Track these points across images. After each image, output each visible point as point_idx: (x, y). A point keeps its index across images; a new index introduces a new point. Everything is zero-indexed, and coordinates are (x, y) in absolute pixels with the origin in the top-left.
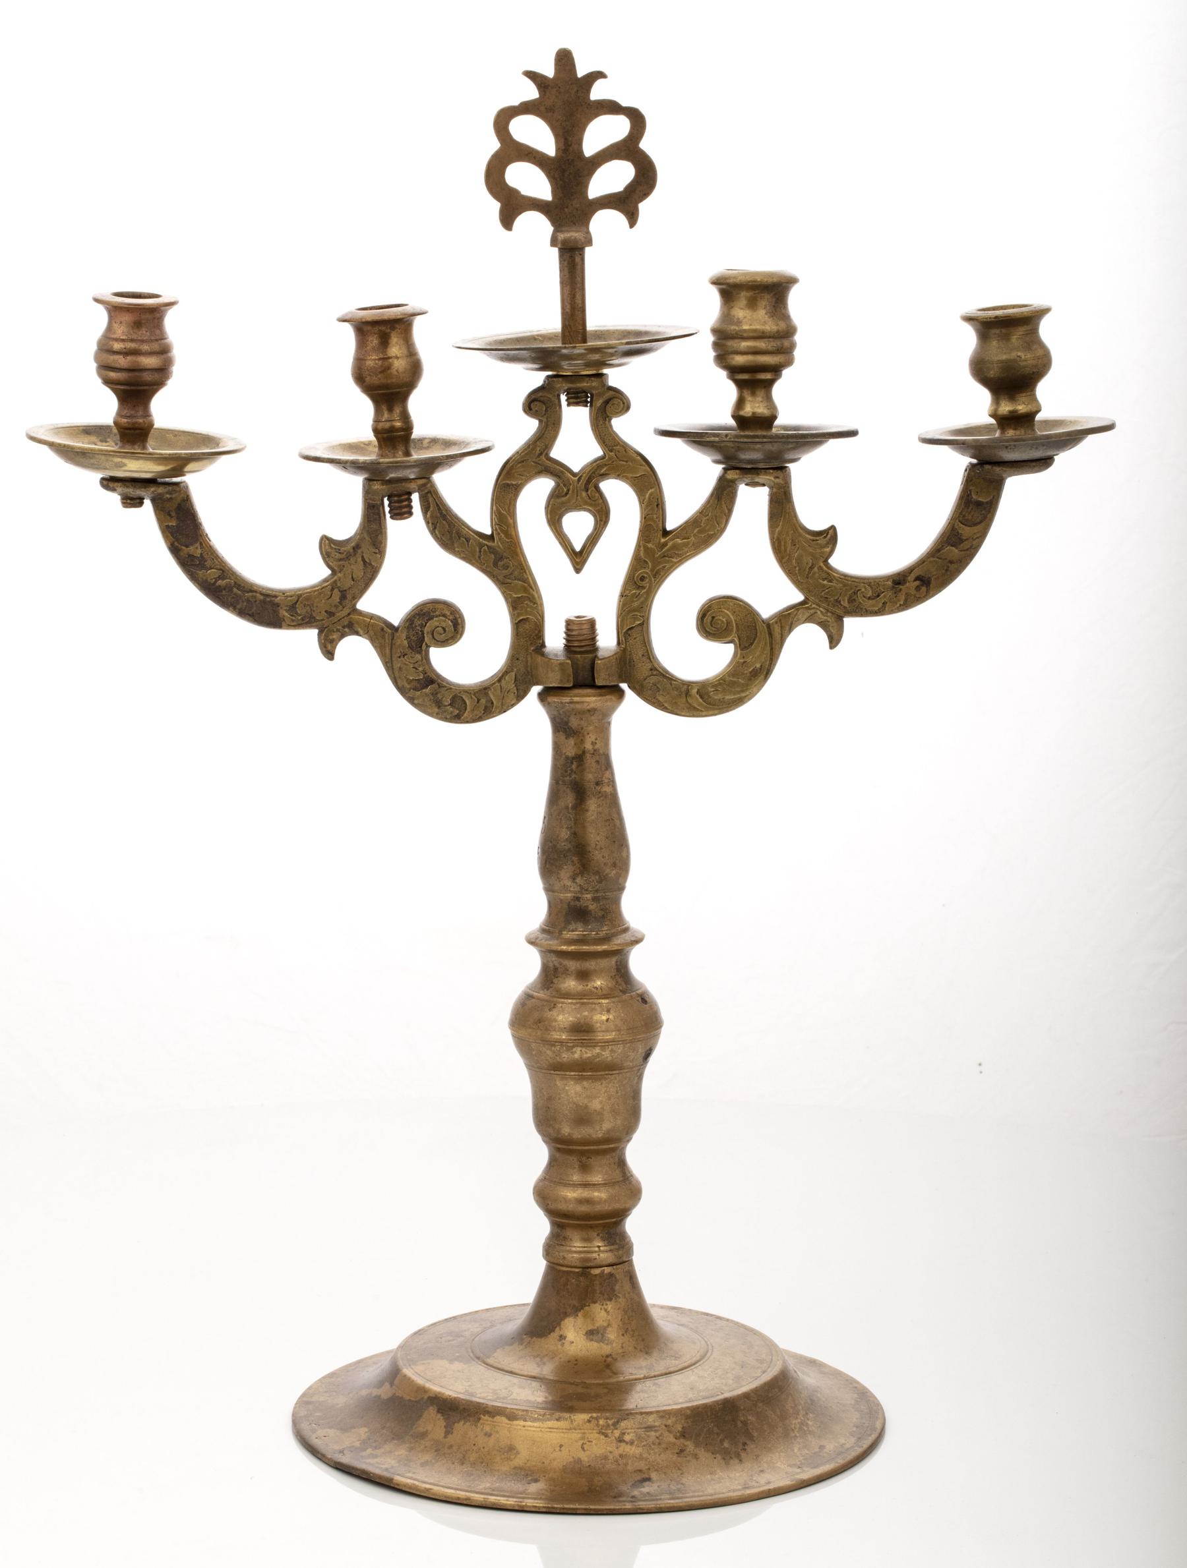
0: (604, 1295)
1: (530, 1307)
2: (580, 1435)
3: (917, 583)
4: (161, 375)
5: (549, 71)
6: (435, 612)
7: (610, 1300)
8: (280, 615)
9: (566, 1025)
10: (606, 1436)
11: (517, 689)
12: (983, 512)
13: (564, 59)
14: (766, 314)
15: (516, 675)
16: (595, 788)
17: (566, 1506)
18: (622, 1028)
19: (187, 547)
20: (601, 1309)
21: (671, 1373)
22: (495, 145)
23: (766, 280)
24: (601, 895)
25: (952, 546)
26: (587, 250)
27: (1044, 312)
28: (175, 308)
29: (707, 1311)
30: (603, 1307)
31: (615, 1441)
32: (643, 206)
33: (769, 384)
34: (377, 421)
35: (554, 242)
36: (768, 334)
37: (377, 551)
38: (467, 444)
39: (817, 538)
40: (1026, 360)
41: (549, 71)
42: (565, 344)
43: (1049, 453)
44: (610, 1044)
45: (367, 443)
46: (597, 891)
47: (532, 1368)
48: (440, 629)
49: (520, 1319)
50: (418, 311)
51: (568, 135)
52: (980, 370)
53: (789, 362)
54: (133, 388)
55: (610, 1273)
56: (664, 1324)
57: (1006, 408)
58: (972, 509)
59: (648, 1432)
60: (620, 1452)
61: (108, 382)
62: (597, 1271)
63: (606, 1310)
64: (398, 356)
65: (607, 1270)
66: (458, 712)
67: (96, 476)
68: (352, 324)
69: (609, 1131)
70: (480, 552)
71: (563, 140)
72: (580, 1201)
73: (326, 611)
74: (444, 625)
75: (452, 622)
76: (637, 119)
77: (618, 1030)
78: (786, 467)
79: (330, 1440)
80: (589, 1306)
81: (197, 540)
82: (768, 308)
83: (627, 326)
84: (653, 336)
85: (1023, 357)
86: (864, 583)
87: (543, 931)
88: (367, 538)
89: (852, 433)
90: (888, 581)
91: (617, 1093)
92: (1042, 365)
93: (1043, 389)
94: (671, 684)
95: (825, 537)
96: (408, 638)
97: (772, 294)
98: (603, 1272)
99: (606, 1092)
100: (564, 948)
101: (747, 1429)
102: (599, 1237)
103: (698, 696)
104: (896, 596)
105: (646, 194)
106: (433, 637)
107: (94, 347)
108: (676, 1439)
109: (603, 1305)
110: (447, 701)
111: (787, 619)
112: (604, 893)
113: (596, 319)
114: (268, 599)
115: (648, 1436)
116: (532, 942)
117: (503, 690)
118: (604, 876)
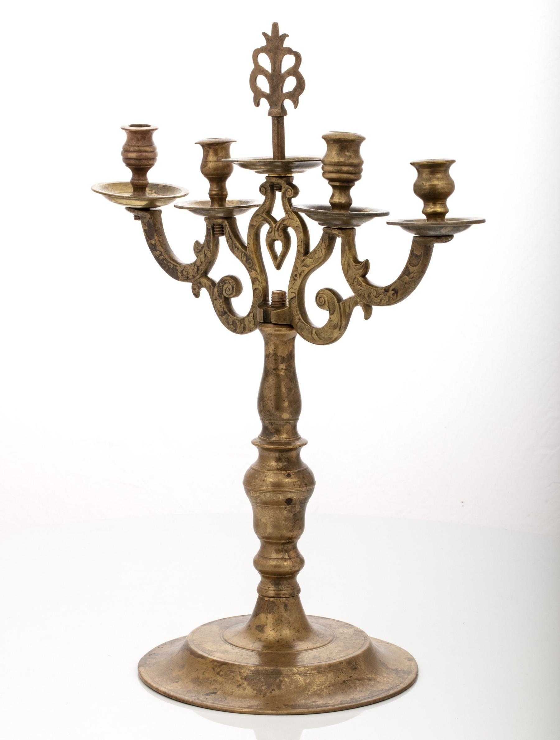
0: (268, 610)
2: (205, 667)
3: (393, 292)
5: (270, 33)
6: (227, 281)
7: (270, 613)
8: (178, 275)
9: (271, 482)
10: (214, 670)
11: (254, 321)
12: (418, 260)
13: (275, 27)
14: (335, 154)
15: (253, 315)
16: (273, 371)
18: (269, 485)
19: (151, 240)
20: (265, 617)
22: (252, 66)
23: (333, 137)
24: (272, 422)
25: (407, 275)
27: (453, 162)
29: (223, 618)
30: (266, 616)
31: (216, 673)
32: (301, 98)
33: (349, 188)
34: (210, 190)
35: (270, 114)
36: (333, 163)
37: (209, 250)
38: (252, 202)
39: (357, 265)
40: (425, 186)
41: (270, 33)
43: (451, 233)
44: (263, 492)
45: (230, 201)
46: (270, 420)
48: (228, 289)
50: (231, 140)
51: (276, 63)
52: (419, 191)
53: (358, 178)
55: (273, 601)
57: (430, 210)
58: (414, 258)
59: (230, 672)
60: (215, 679)
61: (128, 165)
62: (267, 599)
63: (267, 618)
64: (211, 161)
65: (272, 599)
66: (235, 328)
67: (124, 207)
69: (269, 533)
70: (242, 255)
71: (273, 65)
72: (275, 566)
73: (192, 275)
74: (229, 287)
75: (232, 286)
76: (298, 57)
77: (267, 486)
78: (355, 228)
80: (261, 614)
81: (154, 238)
82: (337, 151)
83: (299, 156)
85: (425, 184)
86: (374, 289)
88: (206, 244)
89: (482, 221)
90: (382, 289)
91: (274, 516)
93: (450, 201)
94: (306, 327)
95: (361, 265)
96: (218, 291)
97: (339, 145)
98: (269, 600)
99: (268, 515)
100: (268, 446)
101: (281, 684)
102: (270, 583)
103: (315, 335)
104: (385, 297)
105: (300, 93)
106: (226, 292)
107: (121, 150)
108: (241, 679)
109: (266, 615)
110: (231, 323)
111: (352, 303)
112: (274, 421)
113: (290, 153)
114: (175, 267)
115: (230, 675)
117: (249, 321)
118: (272, 413)
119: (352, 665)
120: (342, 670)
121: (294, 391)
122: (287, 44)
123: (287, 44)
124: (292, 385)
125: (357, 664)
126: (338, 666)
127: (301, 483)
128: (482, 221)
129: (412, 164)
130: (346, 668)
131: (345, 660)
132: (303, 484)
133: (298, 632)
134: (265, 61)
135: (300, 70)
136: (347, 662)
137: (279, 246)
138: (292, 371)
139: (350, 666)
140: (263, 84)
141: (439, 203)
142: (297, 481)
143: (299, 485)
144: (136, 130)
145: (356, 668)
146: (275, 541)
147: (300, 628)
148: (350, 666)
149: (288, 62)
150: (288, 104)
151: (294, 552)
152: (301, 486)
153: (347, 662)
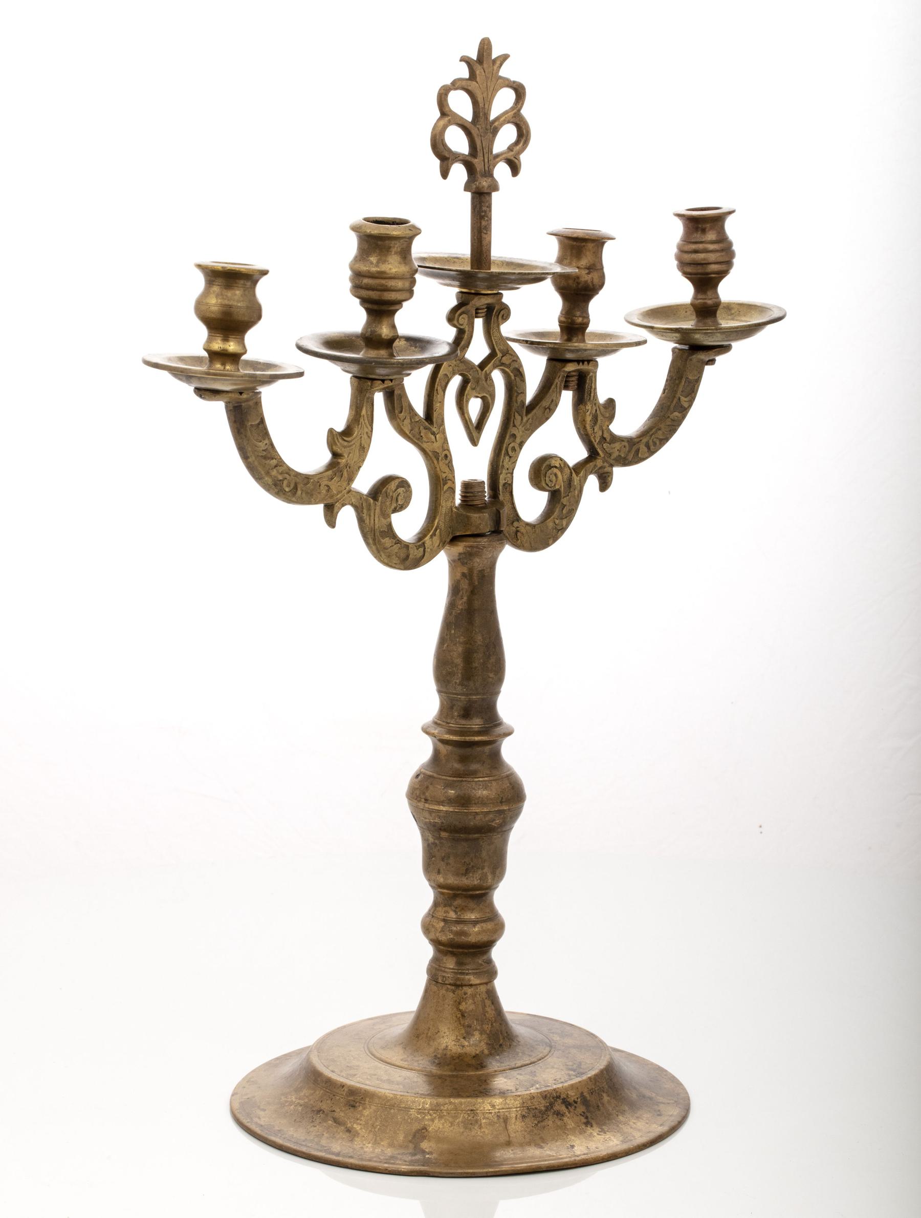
1: (414, 1013)
4: (726, 264)
17: (467, 1171)
21: (525, 1065)
26: (494, 194)
28: (733, 215)
38: (622, 337)
42: (473, 269)
47: (415, 1065)
49: (404, 1025)
54: (703, 276)
56: (518, 1029)
57: (217, 345)
61: (686, 274)
68: (558, 239)
79: (263, 1119)
84: (546, 271)
87: (436, 723)
89: (301, 374)
92: (254, 315)
93: (251, 336)
116: (425, 730)
119: (353, 1099)
120: (334, 1095)
121: (448, 646)
122: (506, 71)
123: (506, 71)
124: (447, 635)
125: (363, 1102)
126: (335, 1088)
127: (420, 794)
128: (301, 374)
129: (199, 266)
130: (342, 1097)
131: (349, 1086)
132: (423, 797)
133: (416, 1037)
134: (461, 104)
135: (525, 112)
136: (349, 1090)
137: (474, 406)
138: (453, 613)
139: (349, 1098)
140: (457, 141)
141: (233, 336)
142: (417, 788)
143: (417, 797)
144: (700, 216)
145: (354, 1106)
146: (478, 892)
147: (423, 1033)
148: (349, 1098)
149: (503, 101)
150: (501, 171)
151: (443, 911)
152: (419, 799)
153: (349, 1090)
